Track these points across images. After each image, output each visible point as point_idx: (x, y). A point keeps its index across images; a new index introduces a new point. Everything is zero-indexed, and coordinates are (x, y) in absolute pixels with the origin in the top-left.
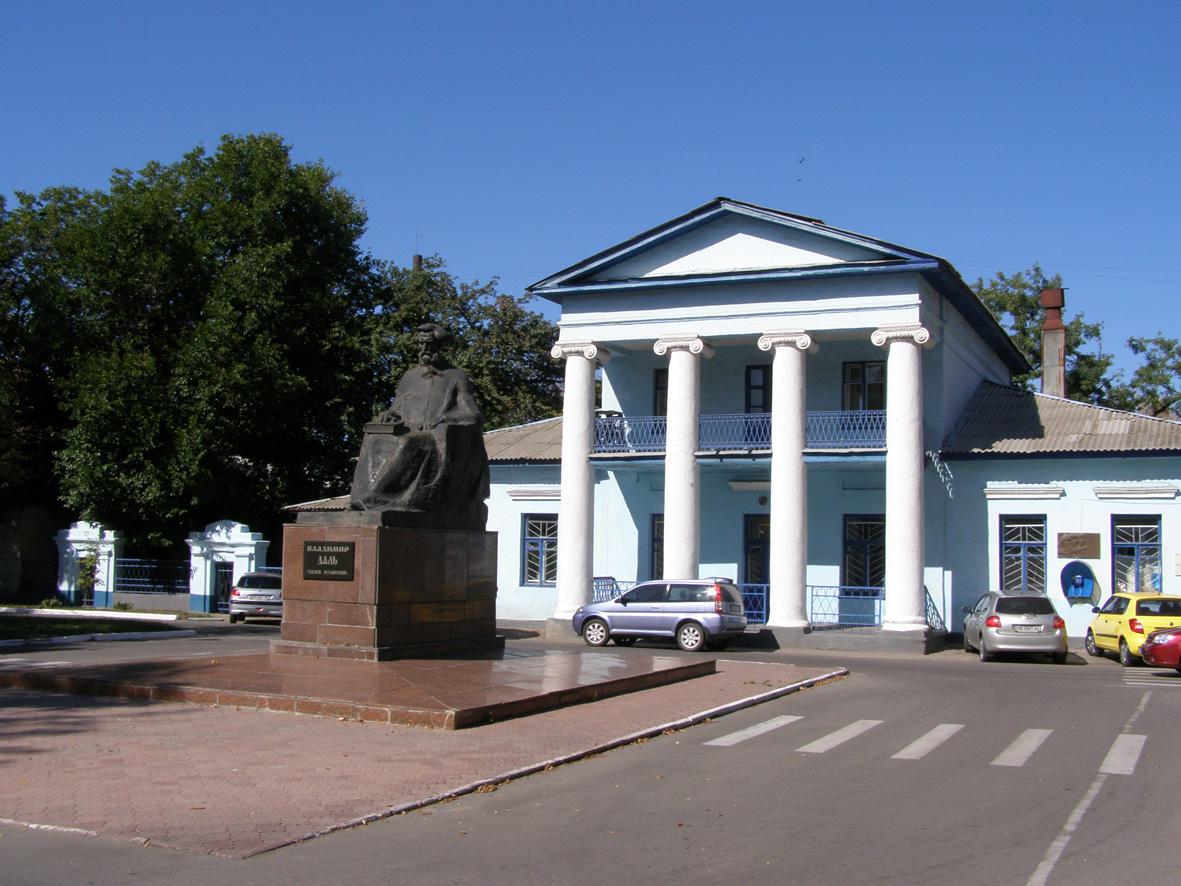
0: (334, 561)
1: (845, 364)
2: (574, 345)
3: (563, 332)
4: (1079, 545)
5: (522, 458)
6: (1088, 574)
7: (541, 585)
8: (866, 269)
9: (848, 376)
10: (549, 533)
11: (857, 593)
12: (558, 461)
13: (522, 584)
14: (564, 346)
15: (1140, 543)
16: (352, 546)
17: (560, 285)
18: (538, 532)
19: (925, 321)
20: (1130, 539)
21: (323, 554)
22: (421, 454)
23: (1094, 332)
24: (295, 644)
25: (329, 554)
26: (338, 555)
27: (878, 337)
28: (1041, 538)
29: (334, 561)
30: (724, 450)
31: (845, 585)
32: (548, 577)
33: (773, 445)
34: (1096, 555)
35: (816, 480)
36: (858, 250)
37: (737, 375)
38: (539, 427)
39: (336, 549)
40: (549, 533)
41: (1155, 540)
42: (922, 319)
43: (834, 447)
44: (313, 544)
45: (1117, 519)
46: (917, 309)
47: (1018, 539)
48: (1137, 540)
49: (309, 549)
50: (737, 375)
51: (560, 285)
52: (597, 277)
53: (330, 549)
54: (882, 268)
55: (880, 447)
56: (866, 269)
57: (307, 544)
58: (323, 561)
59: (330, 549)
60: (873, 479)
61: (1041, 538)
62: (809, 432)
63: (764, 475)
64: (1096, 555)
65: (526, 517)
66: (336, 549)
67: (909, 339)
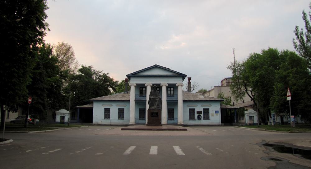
4: (199, 113)
12: (130, 100)
13: (118, 119)
29: (155, 114)
35: (169, 103)
45: (204, 109)
50: (157, 89)
64: (202, 114)
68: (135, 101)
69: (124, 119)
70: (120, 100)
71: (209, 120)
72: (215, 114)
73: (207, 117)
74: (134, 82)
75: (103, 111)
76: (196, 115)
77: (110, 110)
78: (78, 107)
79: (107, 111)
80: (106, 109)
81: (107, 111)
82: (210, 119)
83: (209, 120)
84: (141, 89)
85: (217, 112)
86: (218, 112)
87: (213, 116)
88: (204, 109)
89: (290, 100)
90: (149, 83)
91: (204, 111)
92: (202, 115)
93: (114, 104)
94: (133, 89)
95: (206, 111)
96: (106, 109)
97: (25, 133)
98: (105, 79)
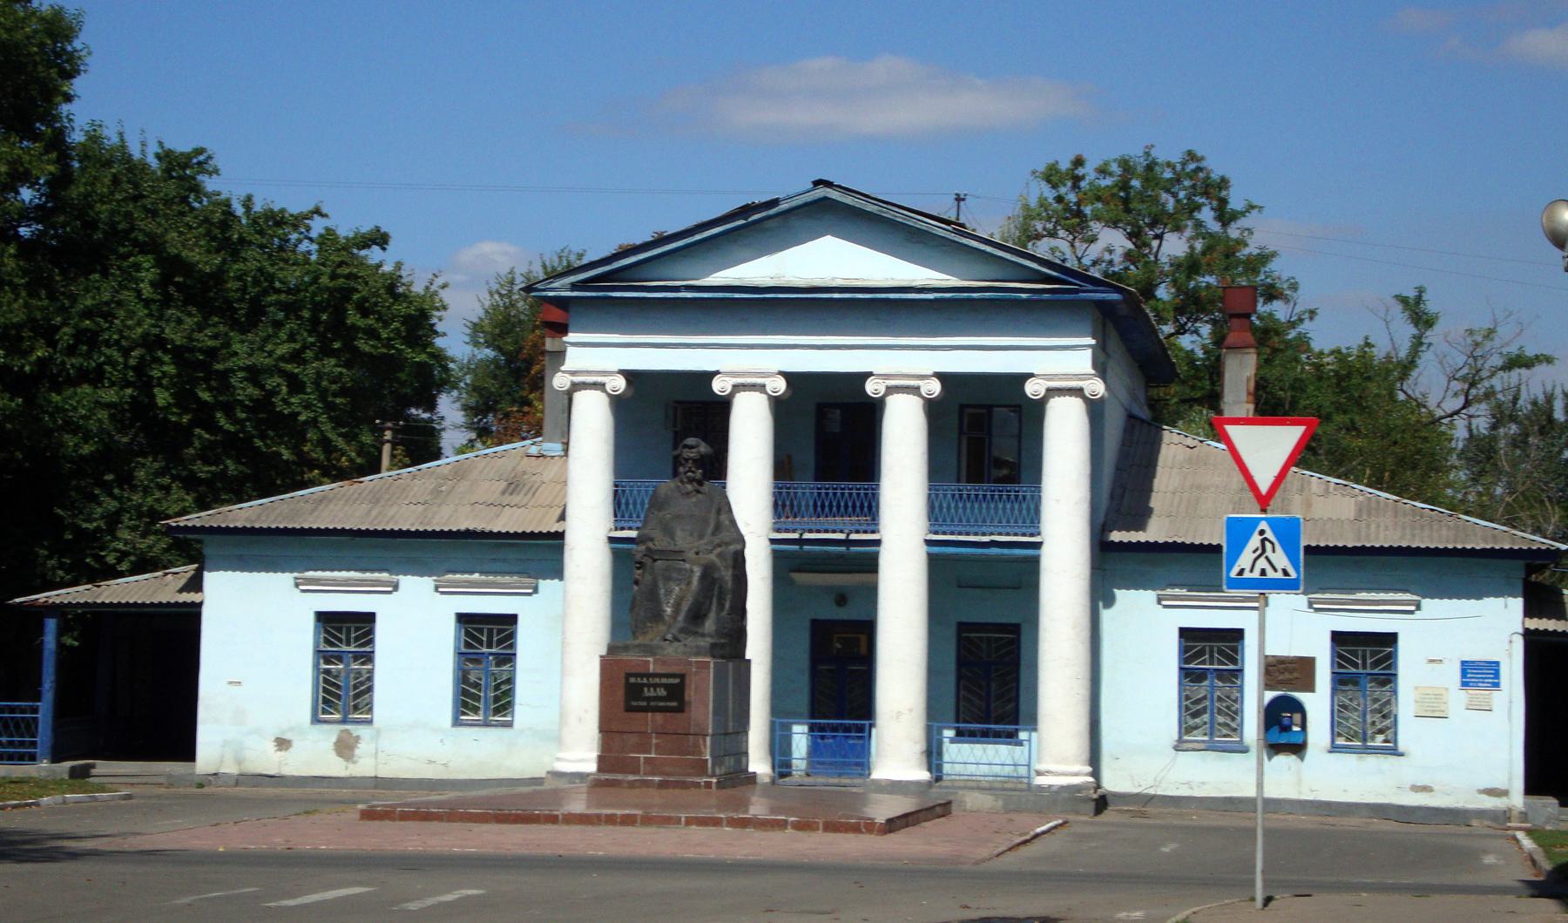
0: (662, 692)
1: (962, 407)
2: (589, 373)
3: (571, 351)
4: (1289, 673)
5: (468, 531)
6: (1299, 708)
7: (486, 724)
8: (1024, 296)
9: (985, 437)
10: (500, 642)
11: (835, 729)
12: (560, 536)
13: (457, 722)
14: (573, 373)
15: (1368, 671)
16: (682, 677)
17: (574, 287)
18: (480, 642)
19: (1101, 368)
20: (1355, 665)
21: (649, 686)
22: (714, 581)
23: (1079, 162)
24: (619, 777)
25: (655, 686)
26: (666, 686)
27: (1036, 387)
28: (1234, 661)
29: (662, 692)
30: (810, 531)
31: (30, 727)
32: (497, 711)
33: (881, 527)
34: (1309, 687)
35: (946, 574)
36: (1394, 559)
37: (830, 435)
38: (446, 471)
39: (664, 681)
40: (357, 638)
41: (1389, 667)
42: (1095, 366)
43: (968, 534)
44: (636, 675)
45: (1338, 638)
46: (1089, 352)
47: (1203, 662)
48: (1364, 667)
49: (632, 680)
50: (830, 435)
51: (574, 287)
52: (627, 274)
53: (657, 680)
54: (1046, 296)
55: (1032, 535)
56: (1024, 296)
57: (628, 676)
58: (647, 693)
59: (657, 680)
60: (1023, 574)
61: (1234, 661)
62: (935, 513)
63: (870, 565)
64: (1309, 687)
65: (464, 619)
66: (664, 681)
67: (1078, 392)
68: (612, 540)
69: (509, 725)
70: (469, 534)
71: (1394, 752)
72: (1457, 698)
73: (1368, 724)
74: (596, 360)
75: (303, 639)
76: (1253, 696)
77: (371, 632)
78: (41, 597)
79: (345, 636)
80: (329, 622)
81: (345, 636)
82: (1402, 747)
83: (1394, 752)
84: (674, 428)
85: (1479, 674)
86: (1497, 675)
87: (1433, 712)
88: (1338, 638)
89: (1529, 612)
90: (750, 369)
91: (1339, 659)
92: (1318, 703)
93: (416, 587)
94: (592, 423)
95: (1366, 660)
96: (329, 622)
97: (30, 805)
98: (1464, 379)
